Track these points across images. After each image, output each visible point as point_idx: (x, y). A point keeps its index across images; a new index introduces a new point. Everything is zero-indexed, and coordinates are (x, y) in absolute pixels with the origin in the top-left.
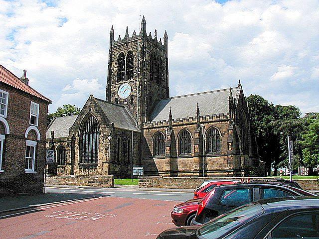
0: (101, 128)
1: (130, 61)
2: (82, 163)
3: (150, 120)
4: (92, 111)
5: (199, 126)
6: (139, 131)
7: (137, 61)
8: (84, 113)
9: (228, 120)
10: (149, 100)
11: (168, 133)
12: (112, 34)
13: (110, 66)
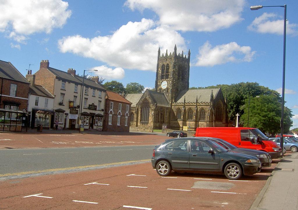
0: (151, 105)
1: (168, 69)
2: (142, 121)
3: (176, 101)
4: (147, 97)
5: (197, 107)
6: (170, 106)
7: (171, 70)
8: (143, 97)
9: (209, 105)
10: (176, 91)
11: (183, 109)
12: (159, 52)
13: (158, 70)
